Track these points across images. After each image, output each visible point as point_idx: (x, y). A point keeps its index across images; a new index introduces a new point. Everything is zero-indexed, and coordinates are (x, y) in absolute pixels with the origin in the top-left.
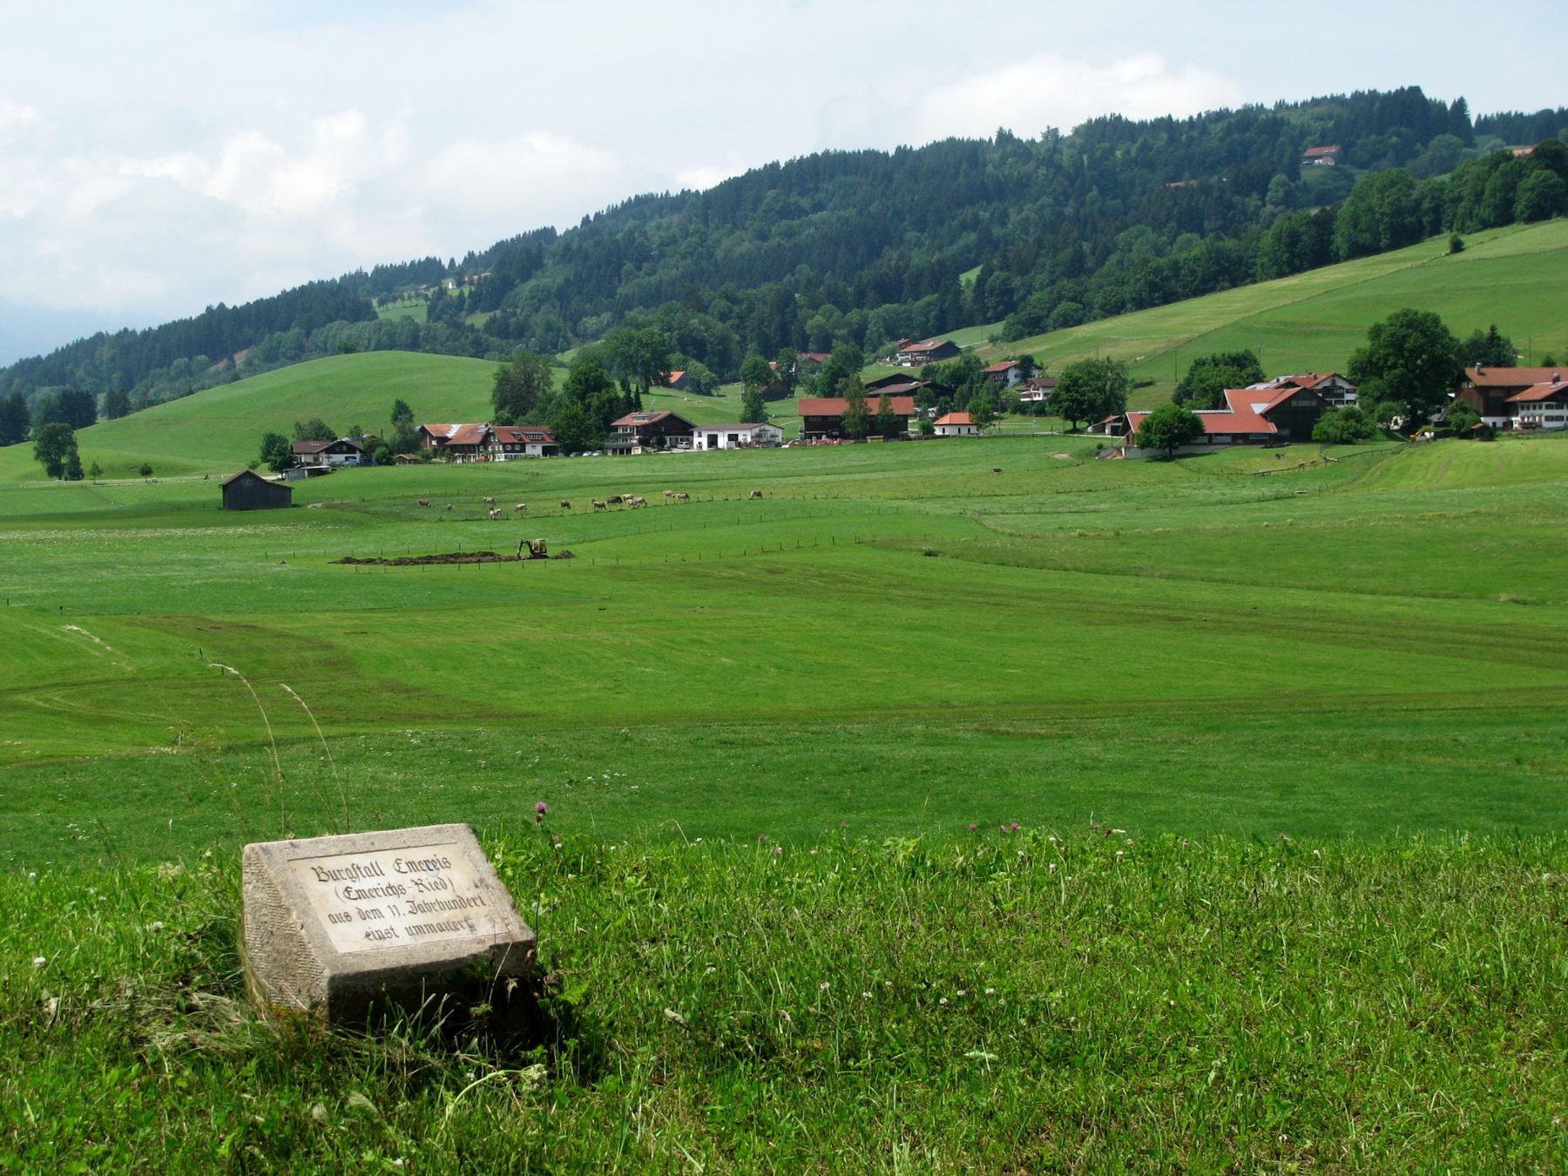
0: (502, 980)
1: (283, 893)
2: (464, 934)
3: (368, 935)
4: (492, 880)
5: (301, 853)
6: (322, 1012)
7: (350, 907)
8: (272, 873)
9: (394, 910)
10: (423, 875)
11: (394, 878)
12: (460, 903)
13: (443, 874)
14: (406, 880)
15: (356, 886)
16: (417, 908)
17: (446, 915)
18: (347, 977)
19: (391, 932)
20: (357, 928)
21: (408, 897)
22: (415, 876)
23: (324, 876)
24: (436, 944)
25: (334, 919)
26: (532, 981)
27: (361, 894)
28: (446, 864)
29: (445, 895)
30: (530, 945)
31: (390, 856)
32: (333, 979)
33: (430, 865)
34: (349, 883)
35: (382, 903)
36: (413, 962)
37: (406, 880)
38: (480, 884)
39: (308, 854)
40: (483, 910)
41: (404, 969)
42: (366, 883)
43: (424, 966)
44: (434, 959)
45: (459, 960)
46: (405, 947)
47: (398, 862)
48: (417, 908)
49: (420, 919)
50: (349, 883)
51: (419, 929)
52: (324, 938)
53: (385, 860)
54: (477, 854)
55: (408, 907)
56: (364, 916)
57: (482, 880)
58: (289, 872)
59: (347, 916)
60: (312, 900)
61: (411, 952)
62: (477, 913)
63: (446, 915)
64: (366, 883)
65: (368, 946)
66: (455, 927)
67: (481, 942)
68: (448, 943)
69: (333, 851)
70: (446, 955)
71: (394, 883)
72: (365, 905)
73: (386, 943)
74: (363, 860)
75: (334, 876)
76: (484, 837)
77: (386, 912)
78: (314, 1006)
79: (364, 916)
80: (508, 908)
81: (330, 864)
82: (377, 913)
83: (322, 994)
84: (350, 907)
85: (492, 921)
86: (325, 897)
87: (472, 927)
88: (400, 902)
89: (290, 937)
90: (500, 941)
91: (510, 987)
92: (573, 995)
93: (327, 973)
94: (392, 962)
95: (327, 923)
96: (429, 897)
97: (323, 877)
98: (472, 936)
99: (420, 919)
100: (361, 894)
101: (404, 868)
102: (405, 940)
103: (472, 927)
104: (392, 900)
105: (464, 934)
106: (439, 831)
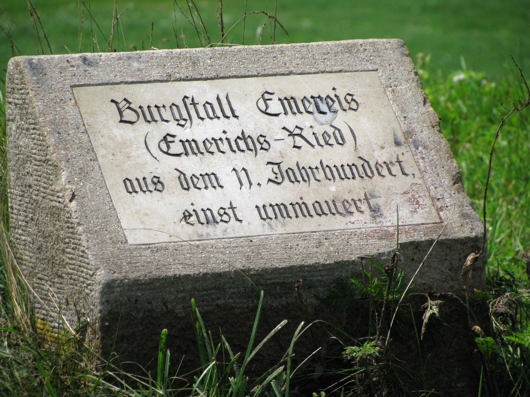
0: (418, 301)
1: (51, 140)
2: (361, 221)
3: (186, 216)
4: (426, 134)
5: (97, 74)
6: (92, 342)
7: (166, 167)
8: (38, 106)
9: (243, 176)
10: (305, 121)
11: (252, 122)
12: (363, 169)
13: (342, 120)
14: (273, 128)
15: (183, 134)
16: (281, 174)
17: (334, 189)
18: (137, 284)
19: (229, 212)
20: (175, 200)
21: (273, 155)
22: (291, 121)
23: (128, 113)
24: (304, 236)
25: (131, 186)
26: (466, 310)
27: (191, 147)
28: (351, 103)
29: (338, 156)
30: (476, 244)
31: (255, 86)
32: (109, 287)
33: (321, 104)
34: (172, 128)
35: (221, 165)
36: (258, 264)
37: (273, 128)
38: (405, 139)
39: (111, 77)
40: (401, 183)
41: (240, 276)
42: (201, 130)
43: (276, 271)
44: (296, 261)
45: (340, 265)
46: (249, 239)
47: (266, 96)
48: (281, 174)
49: (286, 193)
50: (172, 128)
51: (281, 210)
52: (111, 215)
53: (244, 94)
54: (409, 90)
55: (268, 172)
56: (186, 182)
57: (408, 134)
58: (69, 107)
59: (157, 181)
60: (101, 152)
61: (174, 249)
62: (389, 189)
63: (334, 189)
64: (201, 130)
65: (185, 232)
66: (342, 208)
67: (385, 235)
68: (327, 235)
69: (155, 74)
70: (320, 256)
71: (251, 131)
72: (192, 165)
73: (217, 231)
74: (204, 92)
75: (149, 114)
76: (431, 65)
77: (228, 179)
78: (82, 329)
79: (186, 182)
80: (447, 181)
81: (144, 95)
82: (212, 180)
83: (94, 314)
84: (166, 167)
85: (414, 202)
86: (124, 148)
87: (375, 211)
88: (258, 167)
89: (56, 213)
90: (418, 237)
91: (428, 314)
92: (436, 115)
93: (102, 276)
94: (218, 264)
95: (118, 192)
96: (310, 157)
97: (129, 115)
98: (372, 226)
99: (286, 193)
100: (191, 147)
101: (275, 106)
102: (252, 225)
103: (375, 211)
104: (241, 160)
105: (361, 221)
106: (349, 49)
